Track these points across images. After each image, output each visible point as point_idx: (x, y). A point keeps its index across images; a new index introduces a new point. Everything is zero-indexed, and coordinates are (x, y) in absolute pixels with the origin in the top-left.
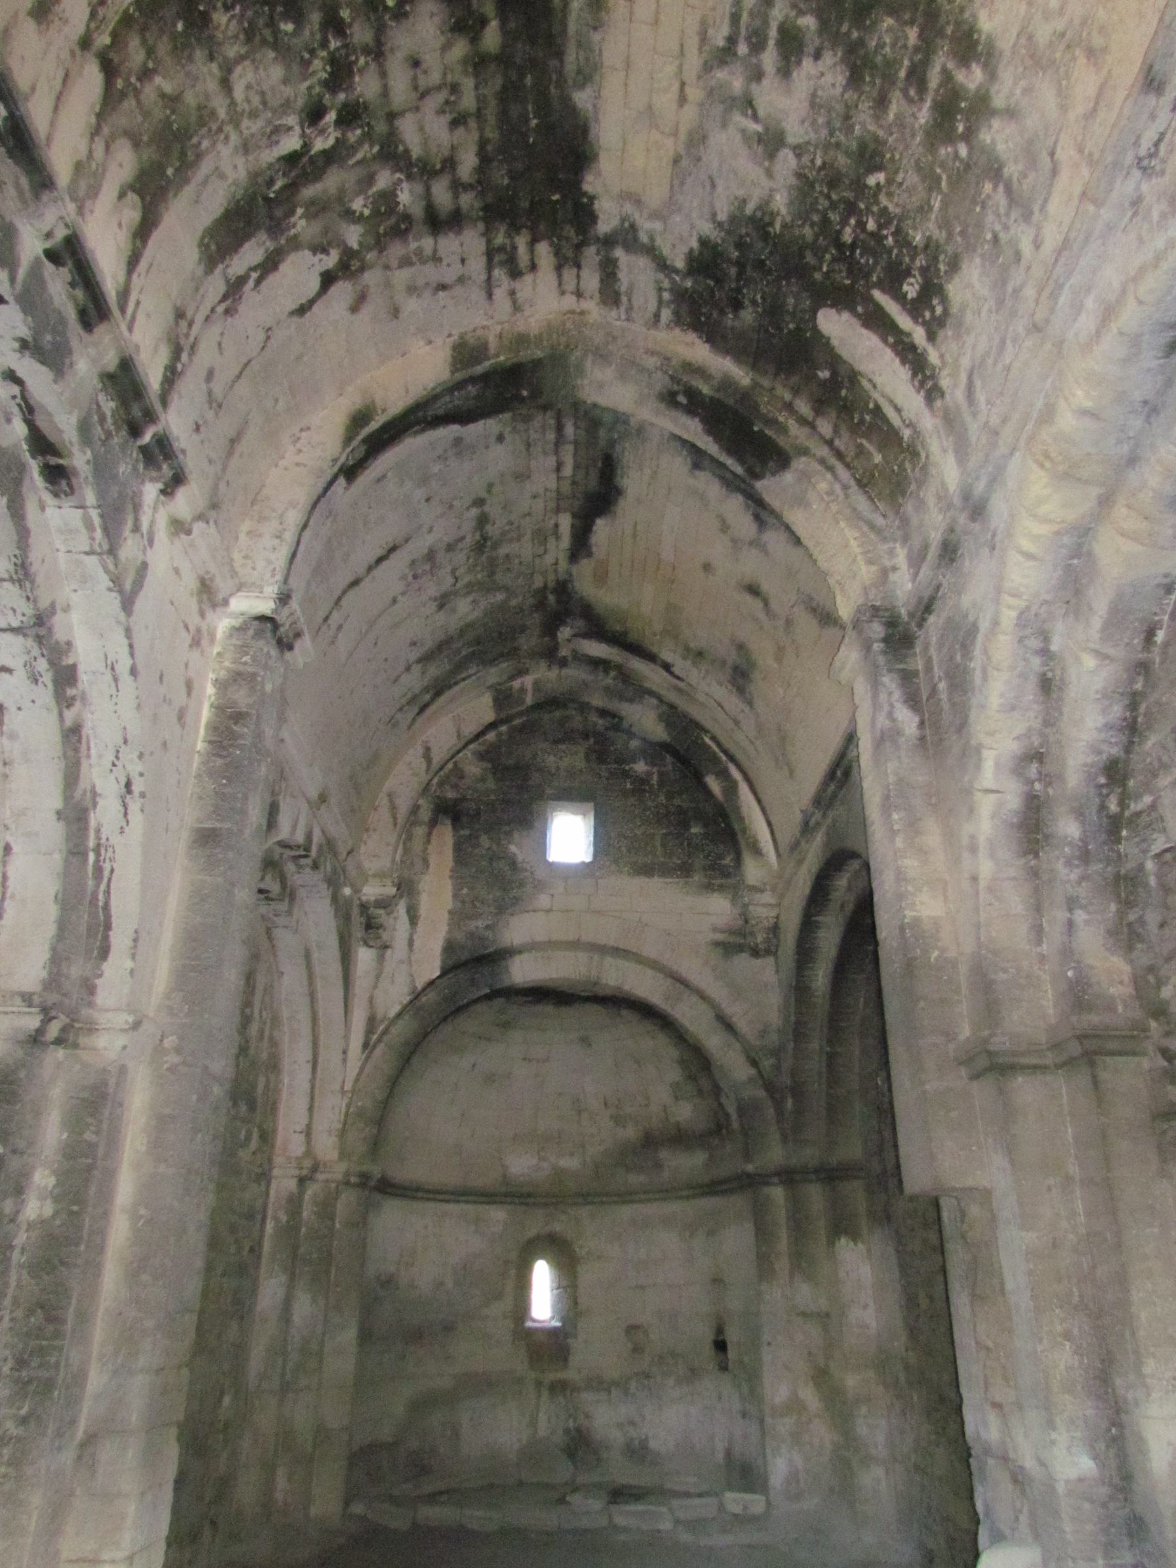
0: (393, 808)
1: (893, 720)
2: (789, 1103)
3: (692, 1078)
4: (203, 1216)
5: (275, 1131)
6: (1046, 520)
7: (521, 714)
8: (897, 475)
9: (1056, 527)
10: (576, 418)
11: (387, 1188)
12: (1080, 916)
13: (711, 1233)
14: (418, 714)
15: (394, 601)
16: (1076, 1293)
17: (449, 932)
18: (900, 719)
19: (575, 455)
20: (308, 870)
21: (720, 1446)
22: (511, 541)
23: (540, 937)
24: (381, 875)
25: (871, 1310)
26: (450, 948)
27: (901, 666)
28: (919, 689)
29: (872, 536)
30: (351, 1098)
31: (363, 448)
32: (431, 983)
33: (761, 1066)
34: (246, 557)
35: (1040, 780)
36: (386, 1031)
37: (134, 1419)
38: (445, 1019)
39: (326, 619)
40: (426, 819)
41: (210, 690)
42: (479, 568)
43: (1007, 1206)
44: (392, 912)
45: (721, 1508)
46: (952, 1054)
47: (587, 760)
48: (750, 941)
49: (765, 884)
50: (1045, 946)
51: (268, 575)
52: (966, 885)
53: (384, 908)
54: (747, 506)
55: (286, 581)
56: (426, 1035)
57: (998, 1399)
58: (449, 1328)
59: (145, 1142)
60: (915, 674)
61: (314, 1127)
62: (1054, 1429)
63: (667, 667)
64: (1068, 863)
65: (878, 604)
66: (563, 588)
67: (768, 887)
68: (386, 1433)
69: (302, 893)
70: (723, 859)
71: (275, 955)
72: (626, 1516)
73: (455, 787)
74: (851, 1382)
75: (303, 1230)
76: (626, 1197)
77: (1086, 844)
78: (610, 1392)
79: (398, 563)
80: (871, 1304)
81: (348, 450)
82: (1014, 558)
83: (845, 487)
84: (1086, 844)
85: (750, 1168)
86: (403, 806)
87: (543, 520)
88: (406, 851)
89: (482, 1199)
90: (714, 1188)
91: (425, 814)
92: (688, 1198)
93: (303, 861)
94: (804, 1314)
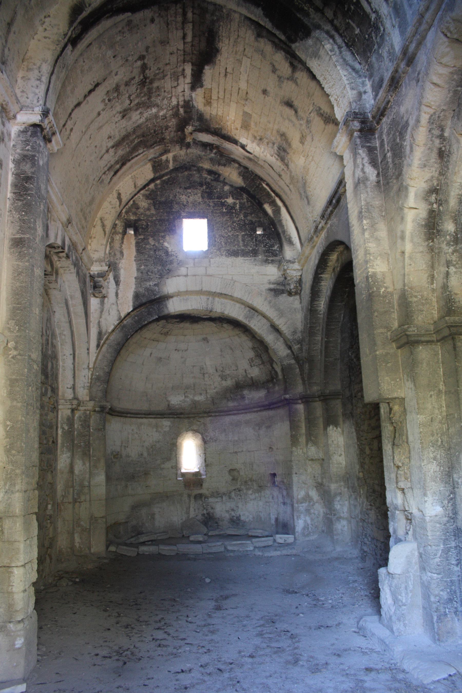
0: (103, 226)
1: (364, 173)
2: (307, 366)
3: (258, 356)
4: (36, 424)
5: (58, 388)
6: (446, 66)
7: (166, 174)
8: (367, 40)
9: (451, 70)
10: (193, 7)
11: (113, 412)
12: (452, 270)
13: (269, 427)
14: (113, 176)
15: (99, 114)
16: (440, 441)
17: (136, 288)
18: (367, 172)
19: (193, 29)
20: (64, 259)
21: (273, 517)
22: (159, 79)
23: (183, 289)
24: (100, 261)
25: (343, 457)
26: (137, 296)
27: (368, 144)
28: (377, 156)
29: (354, 74)
30: (93, 372)
31: (80, 27)
32: (129, 314)
33: (293, 349)
34: (23, 92)
35: (436, 203)
36: (107, 339)
37: (17, 510)
38: (136, 331)
39: (64, 125)
40: (121, 231)
41: (11, 165)
42: (143, 95)
43: (411, 404)
44: (106, 279)
45: (275, 541)
46: (389, 337)
47: (203, 197)
48: (288, 288)
49: (295, 259)
50: (435, 285)
51: (36, 101)
52: (398, 255)
53: (102, 277)
54: (287, 58)
55: (45, 104)
56: (127, 340)
57: (403, 486)
58: (146, 474)
59: (5, 391)
60: (375, 148)
61: (76, 385)
62: (426, 496)
63: (243, 147)
64: (448, 244)
65: (357, 111)
66: (188, 105)
67: (296, 260)
68: (122, 518)
69: (61, 271)
70: (274, 247)
71: (51, 303)
72: (233, 545)
73: (135, 214)
74: (333, 487)
75: (76, 433)
76: (228, 412)
77: (457, 234)
78: (222, 498)
79: (101, 92)
80: (343, 453)
81: (72, 29)
82: (429, 86)
83: (340, 47)
84: (457, 234)
85: (287, 396)
86: (109, 225)
87: (176, 67)
88: (111, 248)
89: (159, 416)
90: (269, 406)
91: (120, 229)
92: (257, 411)
93: (61, 255)
94: (312, 460)
